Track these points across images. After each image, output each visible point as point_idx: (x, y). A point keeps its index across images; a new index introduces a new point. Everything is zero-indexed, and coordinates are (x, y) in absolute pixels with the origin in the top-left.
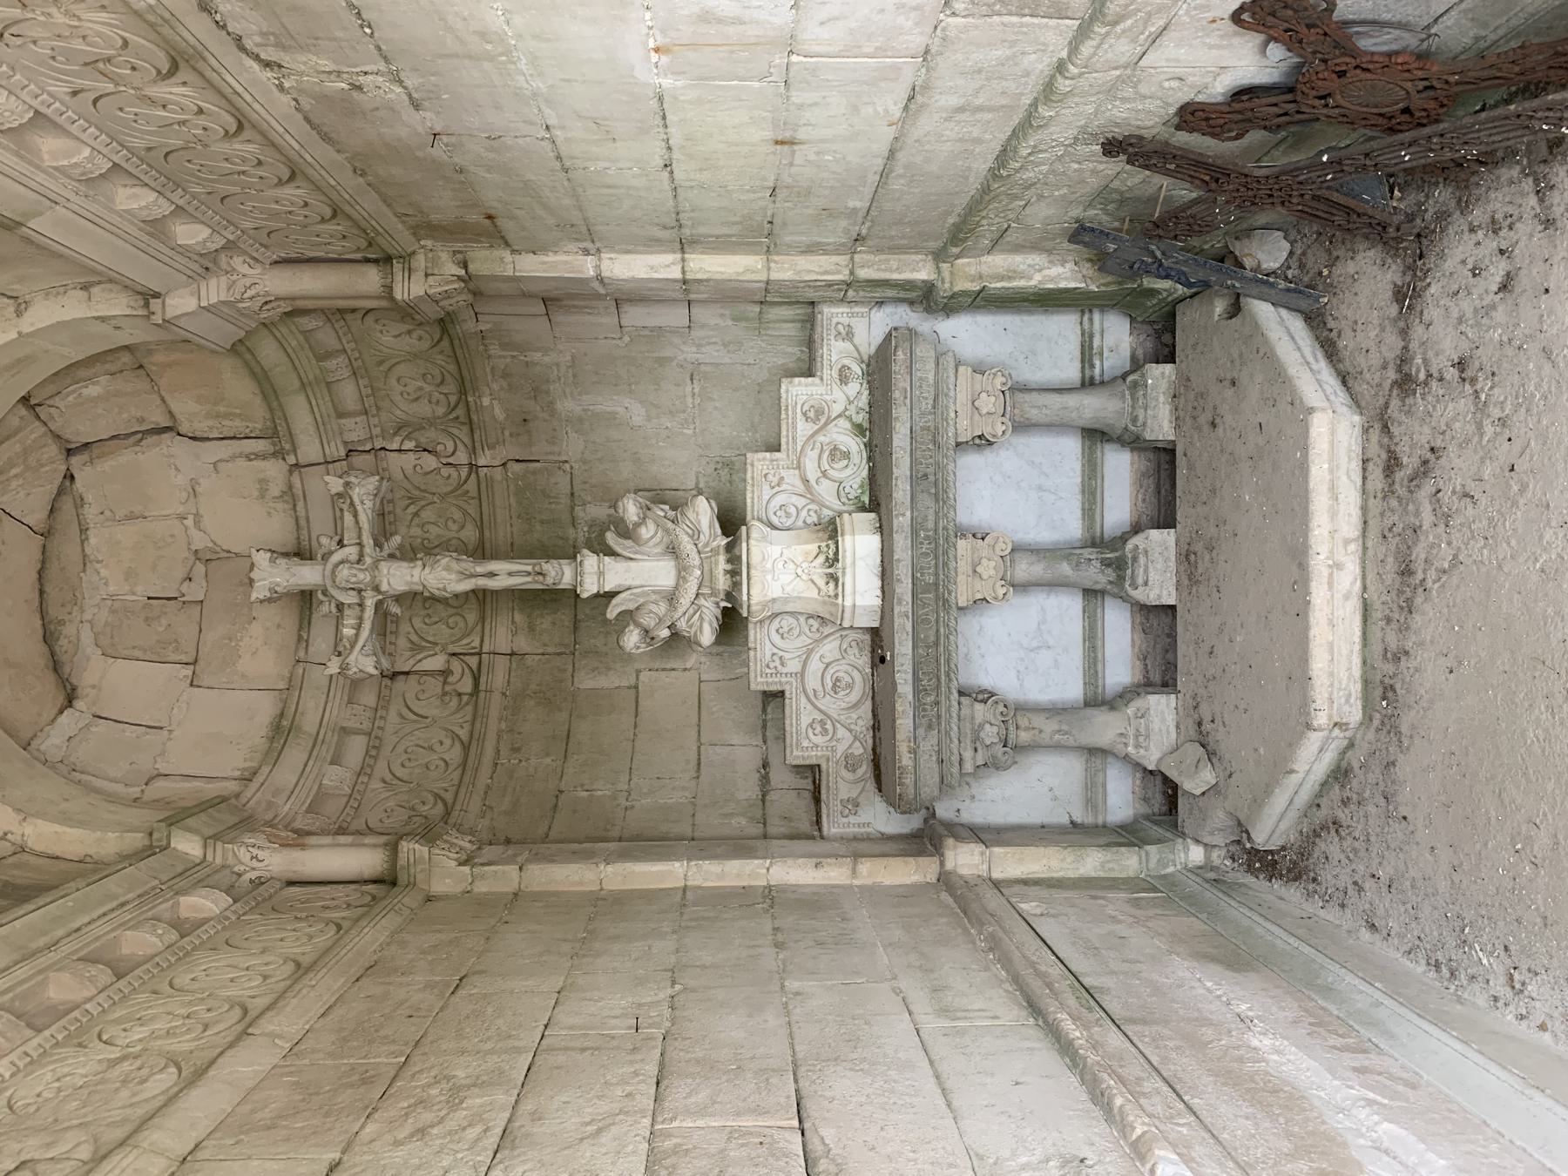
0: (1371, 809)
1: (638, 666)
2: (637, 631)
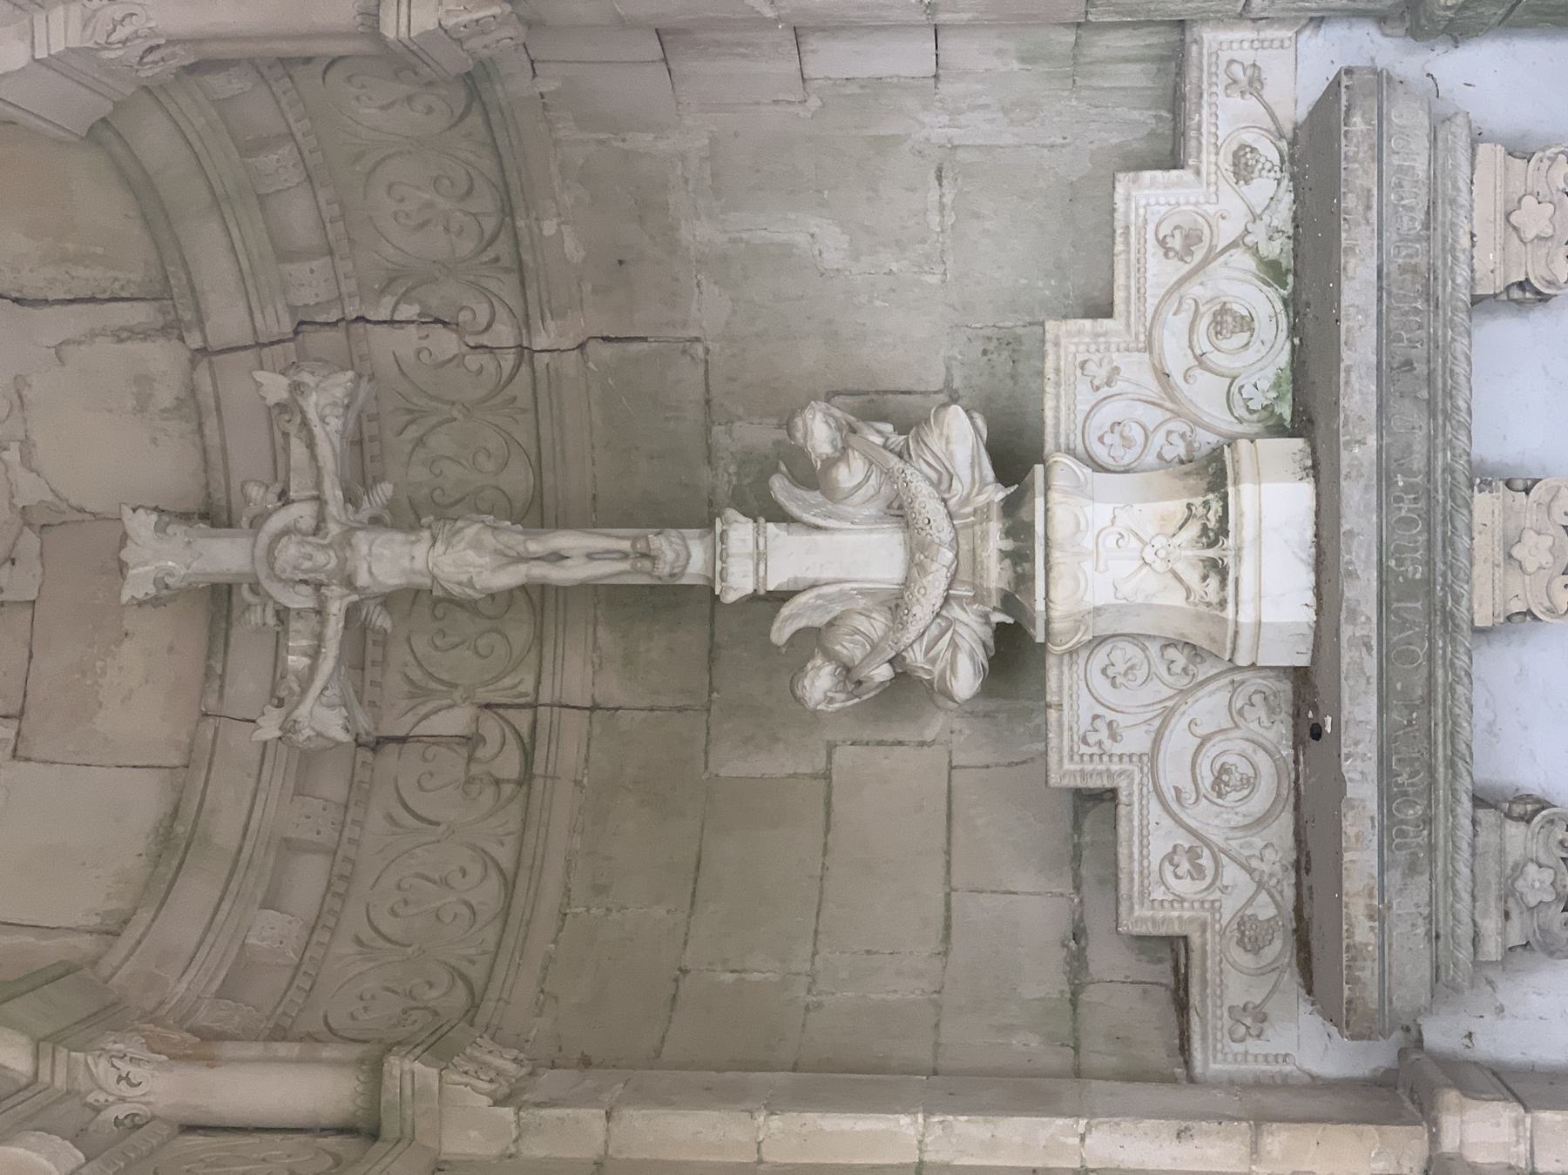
1: (829, 735)
2: (828, 669)
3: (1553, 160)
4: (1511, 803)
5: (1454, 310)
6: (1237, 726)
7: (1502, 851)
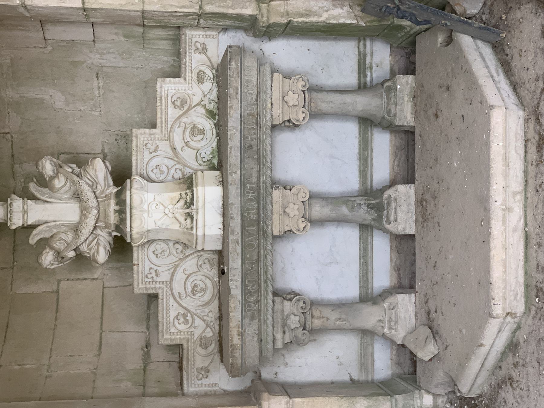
0: (530, 369)
1: (58, 277)
2: (51, 253)
3: (298, 80)
4: (287, 294)
5: (266, 128)
6: (199, 271)
7: (283, 311)
